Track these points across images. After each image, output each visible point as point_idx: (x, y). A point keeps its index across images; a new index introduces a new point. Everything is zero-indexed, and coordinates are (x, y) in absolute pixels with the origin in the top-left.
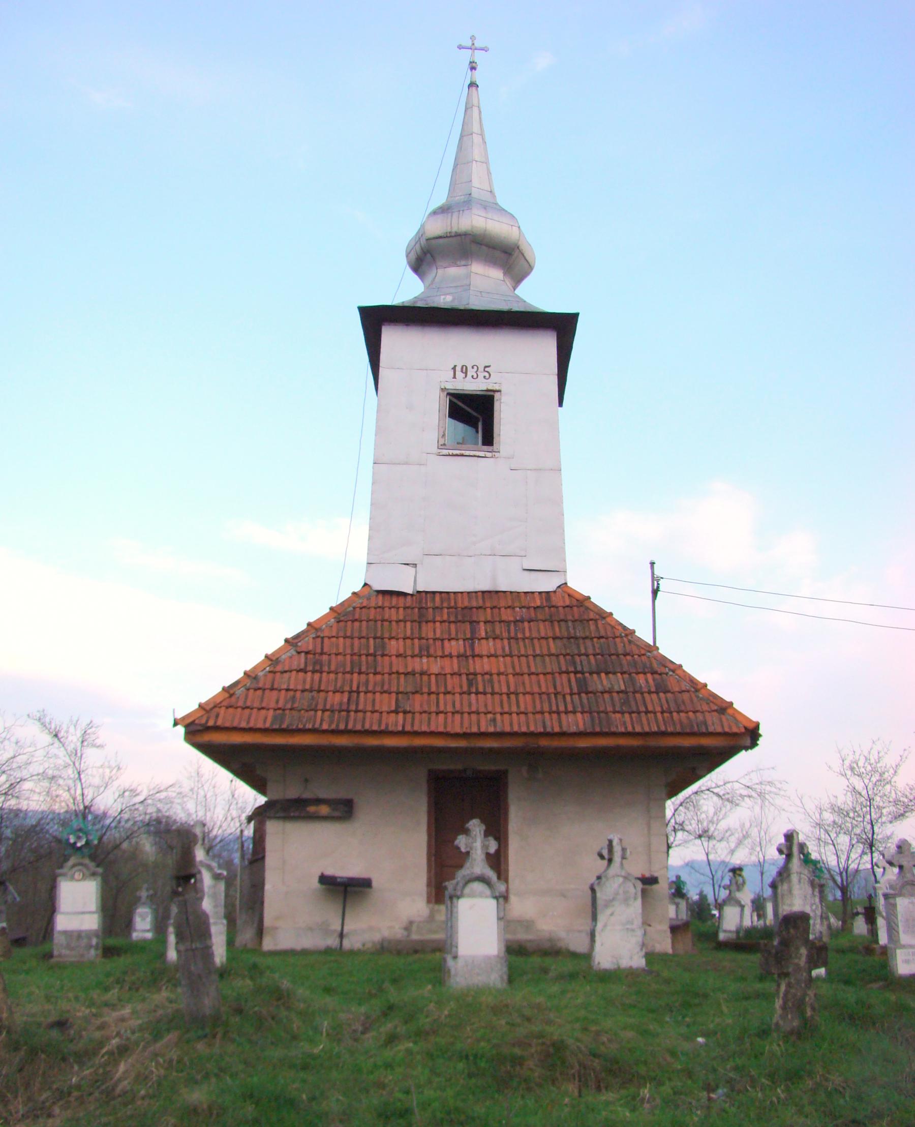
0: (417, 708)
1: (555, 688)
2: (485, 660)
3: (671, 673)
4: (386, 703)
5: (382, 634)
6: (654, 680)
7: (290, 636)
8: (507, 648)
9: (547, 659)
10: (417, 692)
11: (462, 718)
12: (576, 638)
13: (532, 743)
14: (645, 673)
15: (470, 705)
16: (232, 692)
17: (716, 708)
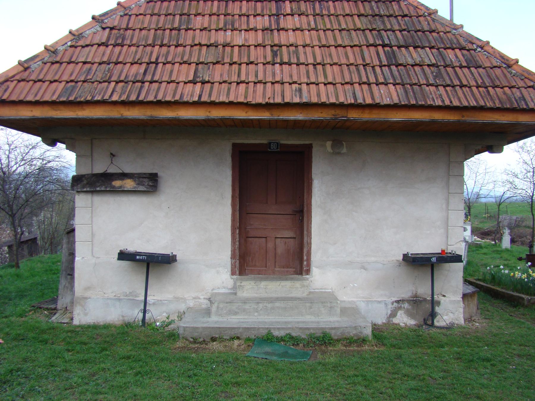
0: (217, 78)
1: (364, 59)
2: (291, 33)
3: (479, 49)
4: (186, 73)
5: (189, 11)
6: (463, 55)
7: (97, 13)
8: (312, 23)
9: (353, 32)
10: (218, 63)
11: (265, 88)
12: (381, 16)
13: (340, 114)
14: (453, 49)
15: (274, 74)
16: (26, 65)
17: (532, 84)
